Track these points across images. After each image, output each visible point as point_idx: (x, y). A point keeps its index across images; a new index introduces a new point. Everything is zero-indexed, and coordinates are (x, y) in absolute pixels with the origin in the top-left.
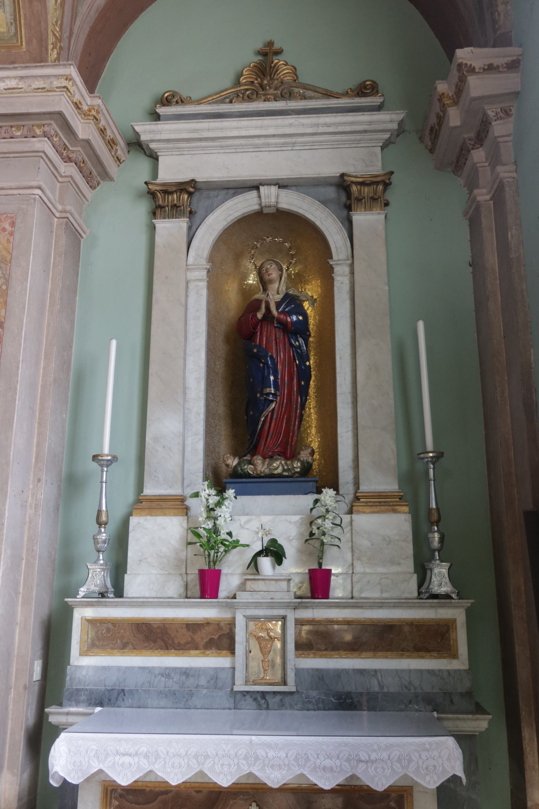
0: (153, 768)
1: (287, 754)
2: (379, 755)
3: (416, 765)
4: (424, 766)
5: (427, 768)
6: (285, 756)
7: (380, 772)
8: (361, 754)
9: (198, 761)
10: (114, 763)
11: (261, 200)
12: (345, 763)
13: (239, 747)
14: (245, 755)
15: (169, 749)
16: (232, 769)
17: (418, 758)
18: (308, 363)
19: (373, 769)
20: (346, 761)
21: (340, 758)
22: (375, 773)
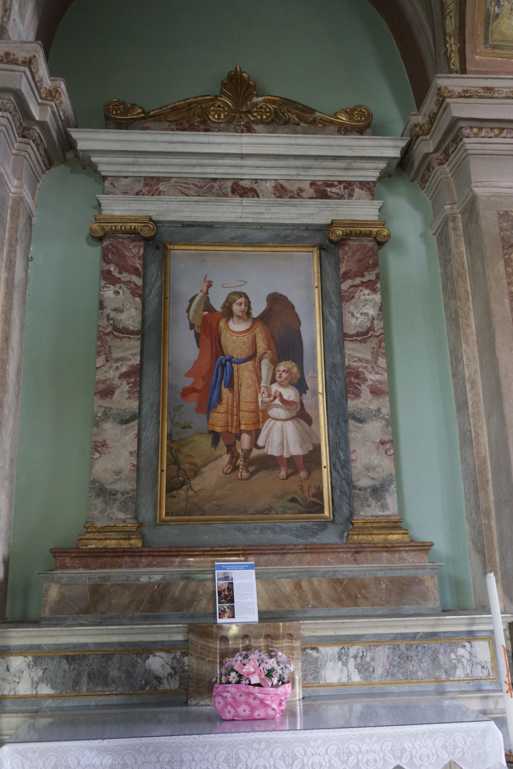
0: (400, 763)
1: (158, 758)
2: (371, 746)
3: (356, 760)
4: (365, 760)
5: (367, 762)
6: (99, 763)
7: (425, 760)
8: (350, 746)
9: (285, 764)
10: (358, 762)
11: (460, 96)
12: (333, 758)
13: (329, 744)
14: (170, 760)
15: (361, 745)
16: (431, 759)
17: (412, 747)
18: (320, 183)
19: (417, 758)
20: (280, 759)
21: (160, 760)
22: (420, 762)
